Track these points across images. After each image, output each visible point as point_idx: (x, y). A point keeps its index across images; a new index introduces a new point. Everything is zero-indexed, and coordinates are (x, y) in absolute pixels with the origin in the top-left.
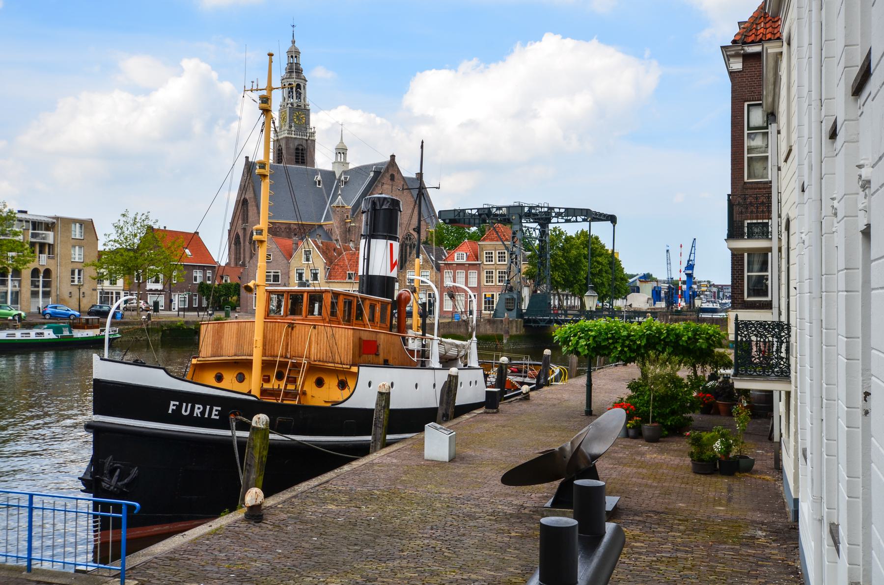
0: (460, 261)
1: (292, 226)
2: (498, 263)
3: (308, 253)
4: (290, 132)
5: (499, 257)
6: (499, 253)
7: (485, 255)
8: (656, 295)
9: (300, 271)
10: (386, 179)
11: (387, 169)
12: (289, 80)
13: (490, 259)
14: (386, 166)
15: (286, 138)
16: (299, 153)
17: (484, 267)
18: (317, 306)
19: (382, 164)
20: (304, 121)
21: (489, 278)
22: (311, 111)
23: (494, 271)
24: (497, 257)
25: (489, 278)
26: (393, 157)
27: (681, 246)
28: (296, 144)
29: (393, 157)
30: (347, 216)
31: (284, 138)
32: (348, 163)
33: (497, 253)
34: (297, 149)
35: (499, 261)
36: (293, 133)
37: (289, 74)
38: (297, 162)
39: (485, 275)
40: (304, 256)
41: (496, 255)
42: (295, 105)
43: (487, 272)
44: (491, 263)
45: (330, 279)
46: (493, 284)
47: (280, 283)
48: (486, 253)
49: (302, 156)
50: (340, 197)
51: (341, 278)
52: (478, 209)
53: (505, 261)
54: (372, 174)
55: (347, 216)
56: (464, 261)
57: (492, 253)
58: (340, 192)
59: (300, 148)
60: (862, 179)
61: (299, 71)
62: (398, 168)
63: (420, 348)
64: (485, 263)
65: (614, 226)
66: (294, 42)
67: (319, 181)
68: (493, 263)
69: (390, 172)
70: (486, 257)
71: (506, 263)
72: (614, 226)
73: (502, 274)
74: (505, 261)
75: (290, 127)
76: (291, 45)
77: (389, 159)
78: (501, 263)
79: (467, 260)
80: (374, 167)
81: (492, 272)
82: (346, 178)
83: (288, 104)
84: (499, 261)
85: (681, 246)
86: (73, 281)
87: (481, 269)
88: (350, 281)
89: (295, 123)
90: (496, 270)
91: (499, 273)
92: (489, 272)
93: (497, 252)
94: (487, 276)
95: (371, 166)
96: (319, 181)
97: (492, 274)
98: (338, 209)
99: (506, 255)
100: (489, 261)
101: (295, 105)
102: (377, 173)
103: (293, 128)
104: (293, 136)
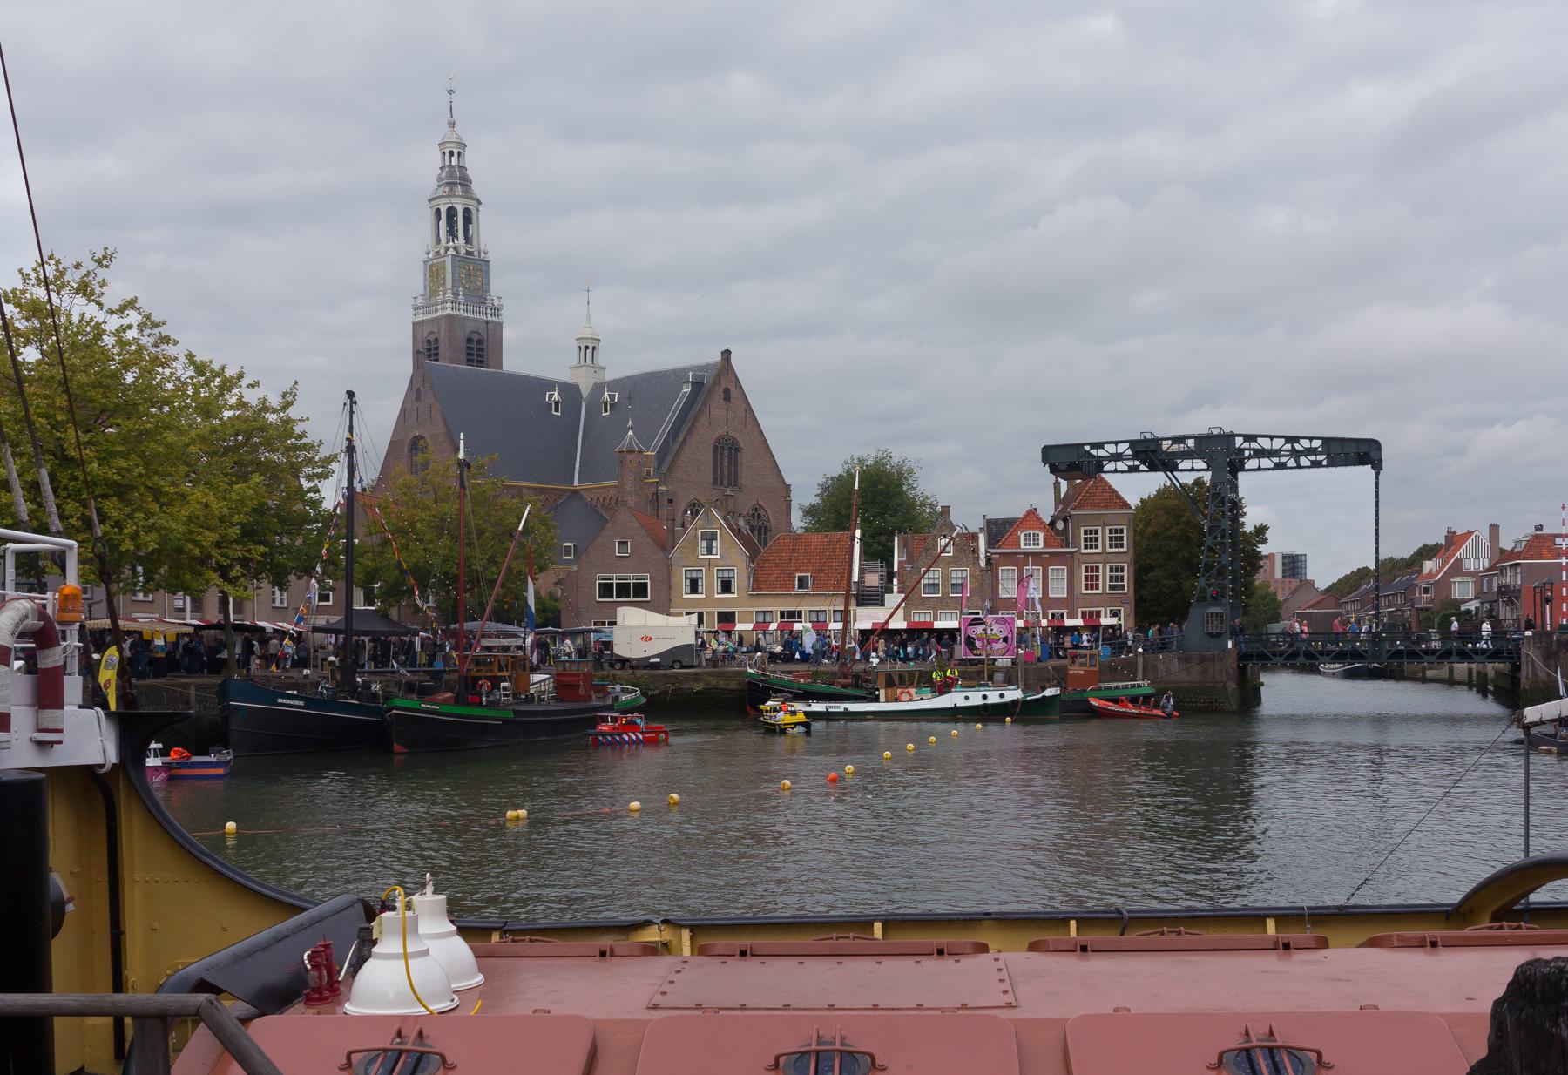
0: (1032, 548)
1: (525, 491)
3: (710, 538)
4: (455, 302)
5: (1111, 539)
6: (1111, 531)
7: (1082, 536)
8: (583, 652)
9: (694, 575)
10: (718, 397)
11: (717, 380)
13: (1091, 542)
14: (714, 372)
15: (449, 316)
16: (472, 348)
17: (1081, 558)
18: (302, 703)
19: (707, 367)
20: (479, 284)
21: (1092, 582)
22: (491, 264)
23: (1101, 566)
24: (1108, 539)
25: (1092, 582)
26: (727, 354)
29: (727, 354)
30: (648, 471)
31: (442, 317)
32: (604, 369)
33: (1107, 531)
34: (469, 340)
35: (1111, 546)
36: (462, 306)
37: (447, 189)
38: (470, 362)
39: (1083, 574)
41: (1103, 535)
42: (463, 251)
43: (1086, 568)
45: (761, 589)
46: (1100, 591)
47: (649, 599)
48: (1086, 532)
49: (478, 355)
50: (630, 433)
51: (784, 587)
53: (1122, 546)
54: (687, 389)
55: (648, 471)
56: (1040, 547)
57: (1096, 532)
58: (630, 423)
59: (476, 337)
61: (465, 182)
62: (736, 377)
64: (1084, 551)
65: (1377, 475)
67: (557, 404)
68: (1099, 550)
69: (724, 385)
70: (1086, 539)
71: (1124, 550)
72: (1377, 475)
73: (1092, 571)
74: (1122, 546)
75: (456, 294)
77: (716, 357)
78: (1089, 551)
79: (1046, 545)
80: (691, 374)
81: (1098, 568)
82: (612, 397)
83: (447, 249)
84: (1111, 546)
86: (274, 601)
87: (1076, 563)
89: (464, 287)
90: (1104, 566)
91: (1111, 571)
92: (1092, 567)
93: (1107, 529)
94: (1086, 577)
95: (685, 371)
96: (557, 404)
97: (1097, 571)
98: (629, 457)
100: (1116, 547)
101: (463, 251)
102: (697, 385)
104: (462, 313)
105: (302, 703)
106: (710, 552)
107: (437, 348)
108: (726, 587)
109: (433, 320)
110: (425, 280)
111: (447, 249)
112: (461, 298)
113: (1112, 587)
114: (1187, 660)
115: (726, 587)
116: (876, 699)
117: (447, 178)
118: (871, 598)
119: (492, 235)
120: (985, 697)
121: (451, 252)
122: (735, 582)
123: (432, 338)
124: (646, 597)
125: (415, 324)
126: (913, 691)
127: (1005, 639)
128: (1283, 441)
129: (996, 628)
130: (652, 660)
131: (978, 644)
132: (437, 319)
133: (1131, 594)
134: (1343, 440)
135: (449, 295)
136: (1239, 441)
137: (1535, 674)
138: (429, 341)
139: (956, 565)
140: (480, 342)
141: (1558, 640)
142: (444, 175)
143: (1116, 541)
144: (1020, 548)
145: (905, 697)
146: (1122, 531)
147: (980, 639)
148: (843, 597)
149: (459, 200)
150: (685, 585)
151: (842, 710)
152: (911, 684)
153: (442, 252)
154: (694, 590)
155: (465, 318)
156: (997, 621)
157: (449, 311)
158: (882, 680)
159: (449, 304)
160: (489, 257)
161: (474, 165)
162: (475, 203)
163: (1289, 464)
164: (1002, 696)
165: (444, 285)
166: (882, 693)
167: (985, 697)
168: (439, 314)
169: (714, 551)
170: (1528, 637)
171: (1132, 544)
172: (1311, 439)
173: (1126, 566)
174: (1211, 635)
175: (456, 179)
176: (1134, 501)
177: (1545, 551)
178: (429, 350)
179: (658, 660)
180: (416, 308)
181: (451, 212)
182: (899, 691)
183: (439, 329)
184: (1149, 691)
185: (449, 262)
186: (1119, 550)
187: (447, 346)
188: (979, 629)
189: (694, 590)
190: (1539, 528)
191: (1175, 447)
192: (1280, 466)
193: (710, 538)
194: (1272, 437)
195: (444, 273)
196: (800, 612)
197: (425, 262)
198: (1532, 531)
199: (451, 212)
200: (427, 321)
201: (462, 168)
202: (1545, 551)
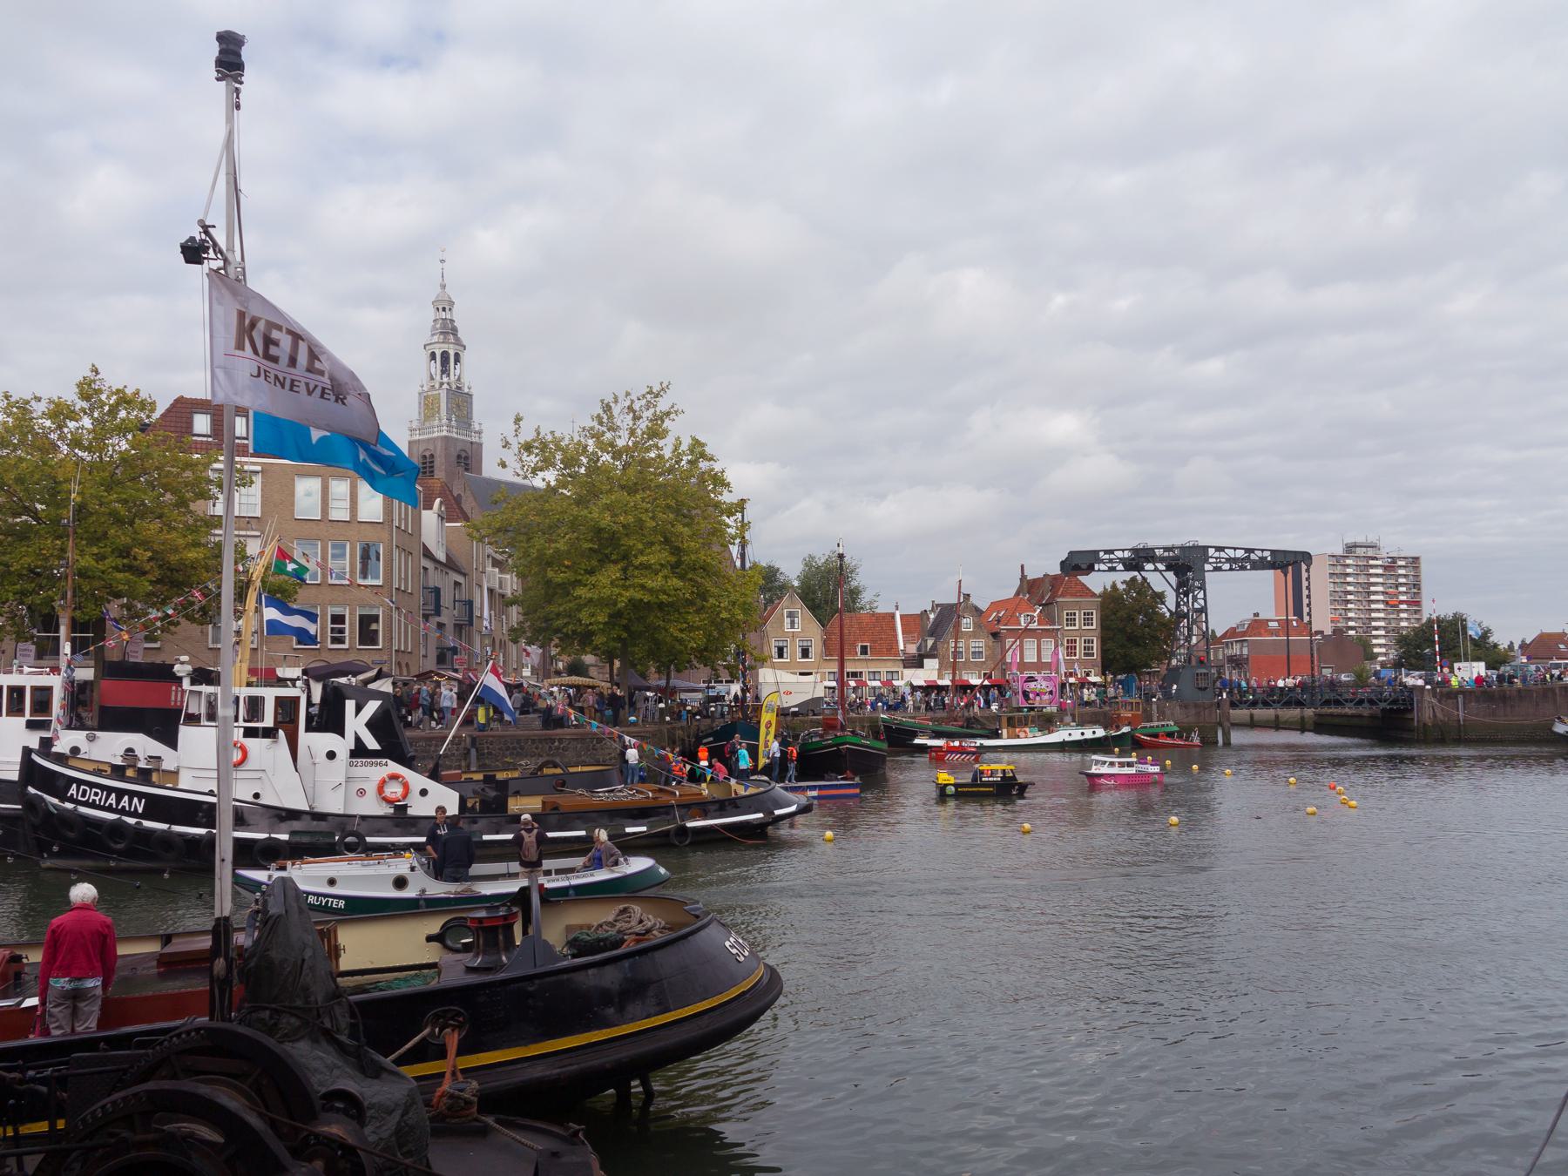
2: (1084, 628)
3: (791, 615)
9: (781, 644)
12: (443, 345)
13: (1071, 621)
15: (446, 437)
18: (711, 739)
25: (1071, 650)
27: (230, 59)
28: (421, 449)
34: (459, 457)
40: (787, 621)
44: (1073, 628)
48: (1067, 614)
52: (1273, 552)
57: (1075, 614)
59: (464, 455)
60: (391, 680)
61: (454, 331)
63: (952, 804)
66: (443, 287)
68: (1077, 627)
70: (1067, 620)
71: (1094, 627)
75: (449, 420)
76: (439, 290)
83: (442, 384)
85: (230, 59)
88: (863, 657)
99: (1094, 616)
101: (454, 387)
103: (453, 423)
104: (455, 435)
105: (711, 739)
106: (793, 627)
107: (433, 462)
108: (805, 653)
109: (428, 440)
110: (420, 408)
111: (442, 384)
112: (453, 423)
113: (1086, 654)
114: (1186, 707)
115: (805, 653)
116: (998, 736)
117: (441, 328)
118: (916, 662)
119: (473, 372)
120: (1083, 734)
121: (445, 386)
122: (812, 651)
123: (427, 454)
124: (377, 644)
125: (410, 442)
126: (1027, 730)
127: (1051, 692)
128: (1243, 551)
129: (1044, 684)
130: (793, 709)
131: (1031, 696)
132: (434, 439)
133: (1099, 659)
134: (1296, 552)
135: (445, 421)
136: (1101, 554)
137: (1435, 716)
138: (425, 457)
139: (975, 638)
140: (466, 458)
141: (1441, 692)
142: (438, 326)
143: (1088, 621)
144: (1020, 625)
145: (1022, 735)
146: (1092, 614)
147: (1032, 692)
148: (837, 663)
149: (451, 346)
150: (774, 651)
151: (978, 744)
152: (1026, 725)
153: (437, 386)
154: (781, 655)
155: (457, 439)
156: (1045, 679)
157: (445, 433)
158: (1004, 721)
159: (445, 428)
160: (473, 391)
161: (459, 316)
162: (462, 348)
163: (1224, 568)
164: (1094, 733)
165: (439, 412)
166: (1005, 732)
167: (1083, 734)
168: (436, 435)
169: (796, 626)
170: (1428, 690)
171: (1099, 622)
172: (1263, 550)
173: (1095, 639)
174: (1200, 689)
175: (448, 330)
176: (1098, 590)
177: (1263, 631)
178: (424, 463)
179: (797, 709)
180: (411, 430)
181: (445, 356)
182: (1017, 730)
183: (435, 447)
184: (1176, 728)
185: (443, 395)
186: (1090, 627)
187: (444, 461)
188: (1032, 685)
189: (781, 655)
190: (1256, 615)
191: (1166, 554)
192: (1243, 568)
193: (791, 615)
194: (1235, 549)
195: (439, 403)
196: (861, 673)
197: (420, 394)
198: (1252, 617)
199: (445, 356)
200: (423, 441)
201: (452, 321)
202: (1263, 631)
